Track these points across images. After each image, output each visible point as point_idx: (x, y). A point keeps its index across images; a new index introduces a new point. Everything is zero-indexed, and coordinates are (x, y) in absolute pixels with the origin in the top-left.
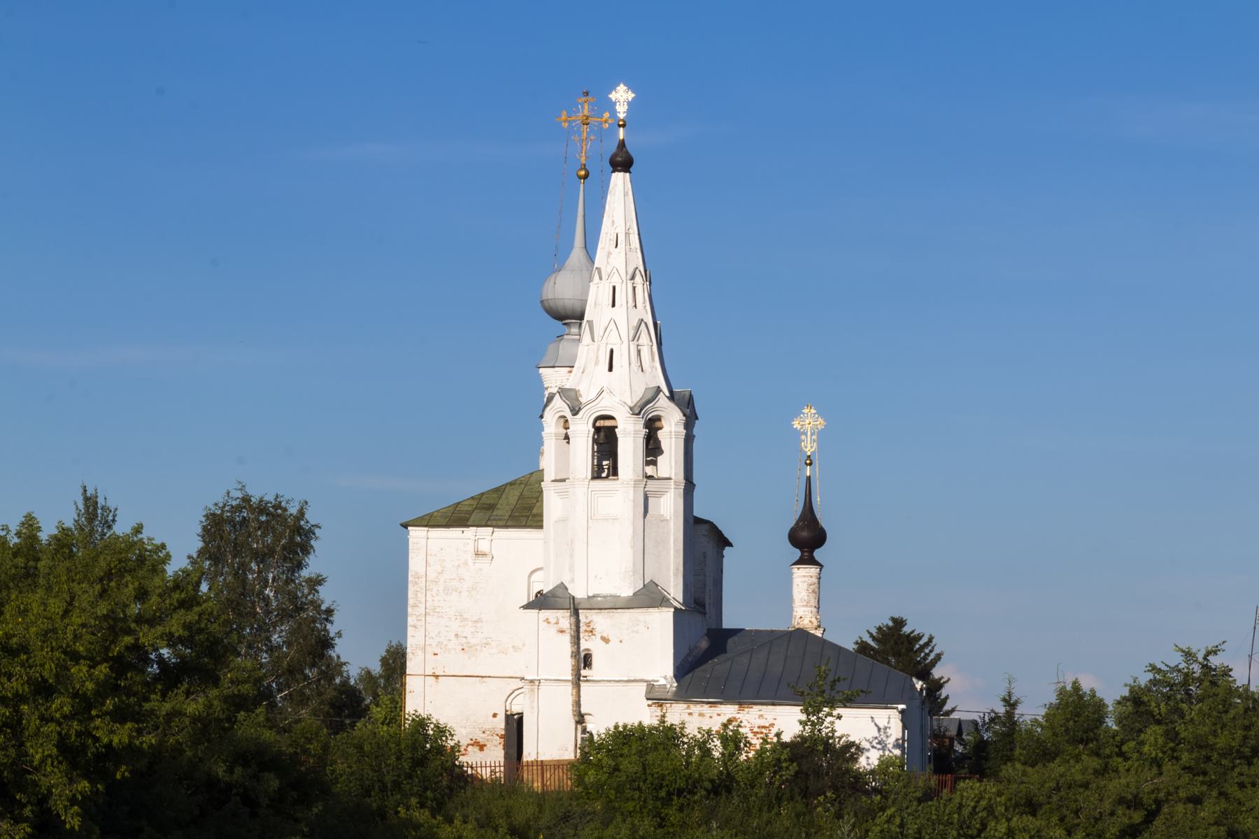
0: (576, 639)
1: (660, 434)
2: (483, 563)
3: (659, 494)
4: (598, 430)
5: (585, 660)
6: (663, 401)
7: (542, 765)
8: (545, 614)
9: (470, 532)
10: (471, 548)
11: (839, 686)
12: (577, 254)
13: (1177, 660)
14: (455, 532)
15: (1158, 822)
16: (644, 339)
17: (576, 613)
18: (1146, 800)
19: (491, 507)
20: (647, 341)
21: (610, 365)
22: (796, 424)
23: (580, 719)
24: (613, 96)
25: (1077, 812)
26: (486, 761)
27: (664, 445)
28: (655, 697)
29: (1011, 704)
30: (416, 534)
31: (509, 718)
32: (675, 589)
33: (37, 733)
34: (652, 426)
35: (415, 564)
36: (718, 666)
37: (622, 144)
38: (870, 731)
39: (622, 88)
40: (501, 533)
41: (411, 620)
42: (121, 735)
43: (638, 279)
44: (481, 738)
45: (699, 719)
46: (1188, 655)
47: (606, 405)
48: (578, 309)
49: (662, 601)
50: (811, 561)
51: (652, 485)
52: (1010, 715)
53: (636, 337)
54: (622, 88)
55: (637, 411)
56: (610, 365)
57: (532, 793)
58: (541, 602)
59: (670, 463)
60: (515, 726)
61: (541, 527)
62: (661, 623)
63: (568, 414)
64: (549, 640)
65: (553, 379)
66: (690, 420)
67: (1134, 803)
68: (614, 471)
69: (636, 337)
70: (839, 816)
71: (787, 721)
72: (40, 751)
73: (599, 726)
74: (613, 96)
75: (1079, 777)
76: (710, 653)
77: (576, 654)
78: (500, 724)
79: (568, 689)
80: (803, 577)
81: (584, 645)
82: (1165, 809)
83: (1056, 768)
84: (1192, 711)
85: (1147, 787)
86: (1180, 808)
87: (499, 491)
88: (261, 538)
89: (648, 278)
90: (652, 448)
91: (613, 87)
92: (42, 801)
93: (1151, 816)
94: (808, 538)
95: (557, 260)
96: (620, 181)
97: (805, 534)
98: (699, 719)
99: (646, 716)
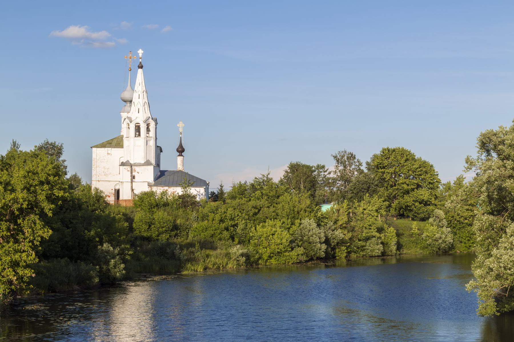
0: (132, 173)
1: (150, 127)
2: (109, 156)
3: (150, 140)
4: (136, 126)
5: (133, 177)
6: (150, 120)
7: (126, 201)
8: (124, 167)
9: (106, 149)
10: (106, 152)
11: (190, 182)
12: (129, 87)
13: (261, 176)
14: (103, 149)
15: (261, 212)
16: (146, 106)
17: (131, 167)
18: (258, 207)
19: (111, 143)
20: (146, 106)
21: (138, 112)
22: (178, 125)
23: (133, 190)
24: (138, 52)
25: (243, 210)
26: (111, 200)
27: (151, 130)
28: (150, 185)
29: (222, 186)
30: (94, 149)
31: (115, 190)
32: (153, 161)
33: (40, 193)
34: (148, 125)
35: (94, 156)
36: (163, 178)
37: (141, 63)
38: (198, 192)
39: (140, 50)
40: (113, 149)
41: (93, 169)
42: (61, 194)
43: (145, 93)
44: (109, 195)
45: (158, 190)
46: (263, 176)
47: (138, 121)
48: (129, 99)
49: (151, 164)
50: (182, 155)
51: (148, 139)
52: (221, 189)
53: (144, 105)
54: (140, 50)
55: (145, 122)
56: (138, 112)
57: (124, 207)
58: (123, 164)
59: (152, 134)
60: (118, 192)
61: (122, 146)
62: (151, 169)
63: (129, 123)
64: (126, 172)
65: (124, 115)
66: (156, 124)
67: (255, 208)
68: (139, 135)
69: (144, 105)
70: (192, 211)
71: (179, 191)
72: (42, 197)
73: (137, 192)
74: (138, 52)
75: (243, 202)
76: (161, 176)
77: (131, 176)
78: (113, 191)
79: (130, 184)
80: (180, 159)
81: (133, 174)
82: (262, 209)
83: (237, 200)
84: (265, 188)
85: (258, 204)
86: (265, 209)
87: (112, 140)
88: (52, 150)
89: (146, 92)
90: (148, 130)
91: (138, 50)
92: (43, 209)
93: (259, 210)
94: (181, 150)
95: (124, 89)
96: (140, 70)
97: (180, 149)
98: (158, 190)
99: (147, 189)
